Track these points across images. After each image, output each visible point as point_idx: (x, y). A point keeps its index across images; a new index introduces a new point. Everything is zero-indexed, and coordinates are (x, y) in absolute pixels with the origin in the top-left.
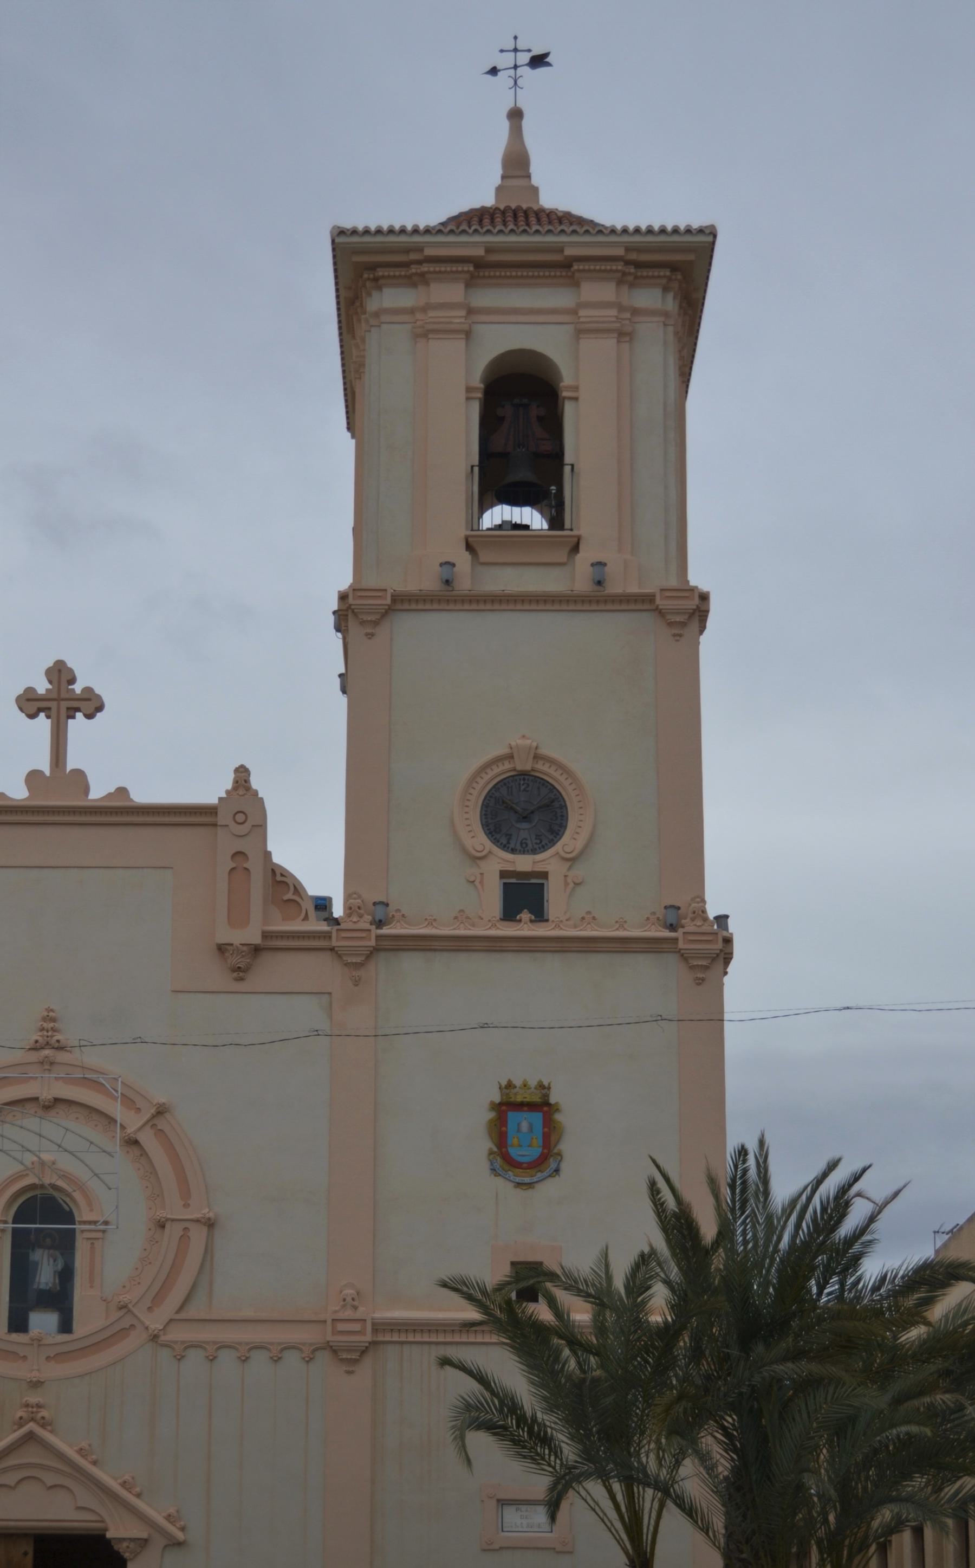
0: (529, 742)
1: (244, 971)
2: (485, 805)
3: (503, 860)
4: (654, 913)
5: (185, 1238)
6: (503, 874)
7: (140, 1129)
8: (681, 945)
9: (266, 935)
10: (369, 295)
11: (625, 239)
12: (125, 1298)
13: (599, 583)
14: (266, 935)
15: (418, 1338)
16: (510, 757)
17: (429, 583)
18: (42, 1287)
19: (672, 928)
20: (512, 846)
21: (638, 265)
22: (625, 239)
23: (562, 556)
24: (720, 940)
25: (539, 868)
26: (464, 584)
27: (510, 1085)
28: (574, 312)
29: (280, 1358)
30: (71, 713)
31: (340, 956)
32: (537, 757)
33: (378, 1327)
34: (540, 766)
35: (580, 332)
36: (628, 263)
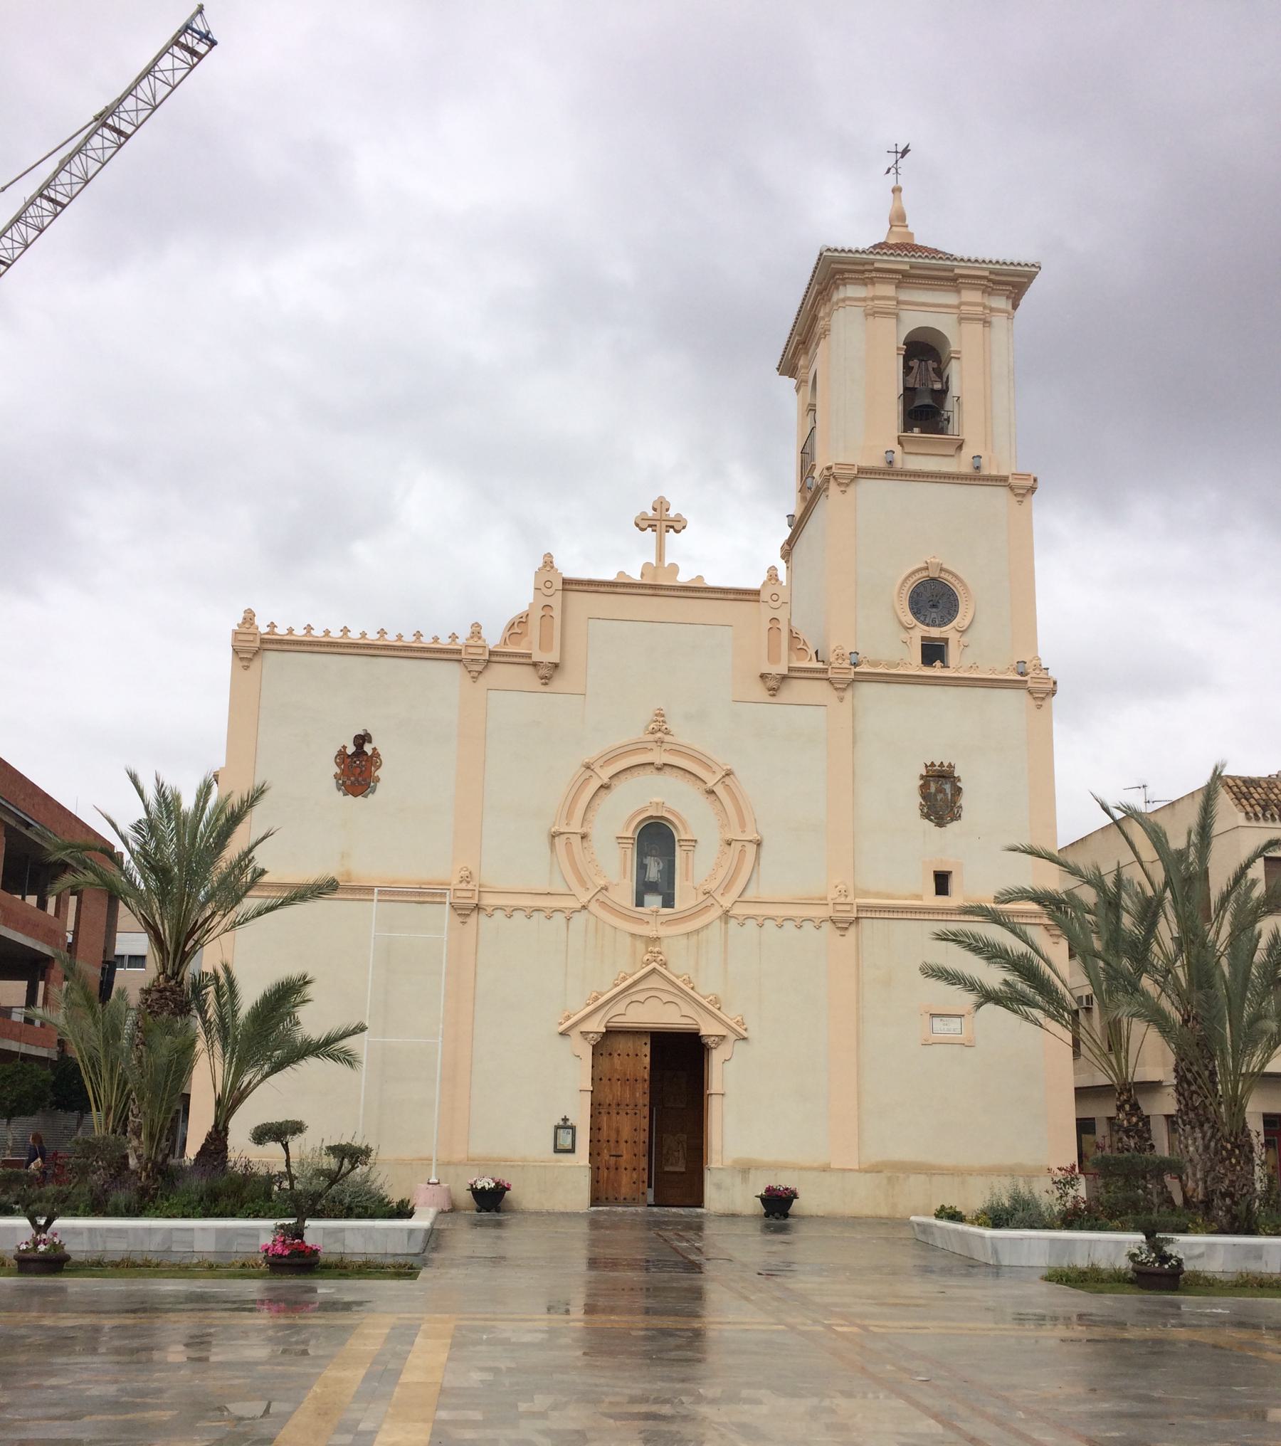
0: (937, 560)
1: (776, 691)
2: (911, 597)
3: (921, 631)
4: (1012, 665)
5: (742, 851)
6: (923, 638)
7: (715, 785)
8: (1029, 685)
9: (790, 669)
10: (837, 288)
11: (991, 266)
12: (707, 887)
13: (978, 468)
14: (790, 669)
15: (882, 915)
16: (927, 568)
17: (878, 462)
18: (651, 880)
19: (1022, 674)
20: (927, 622)
21: (995, 282)
22: (991, 266)
23: (952, 451)
24: (259, 641)
25: (943, 636)
26: (898, 464)
27: (933, 764)
28: (958, 307)
29: (820, 927)
30: (668, 529)
31: (832, 684)
32: (942, 570)
33: (860, 908)
34: (943, 575)
35: (961, 320)
36: (989, 280)
